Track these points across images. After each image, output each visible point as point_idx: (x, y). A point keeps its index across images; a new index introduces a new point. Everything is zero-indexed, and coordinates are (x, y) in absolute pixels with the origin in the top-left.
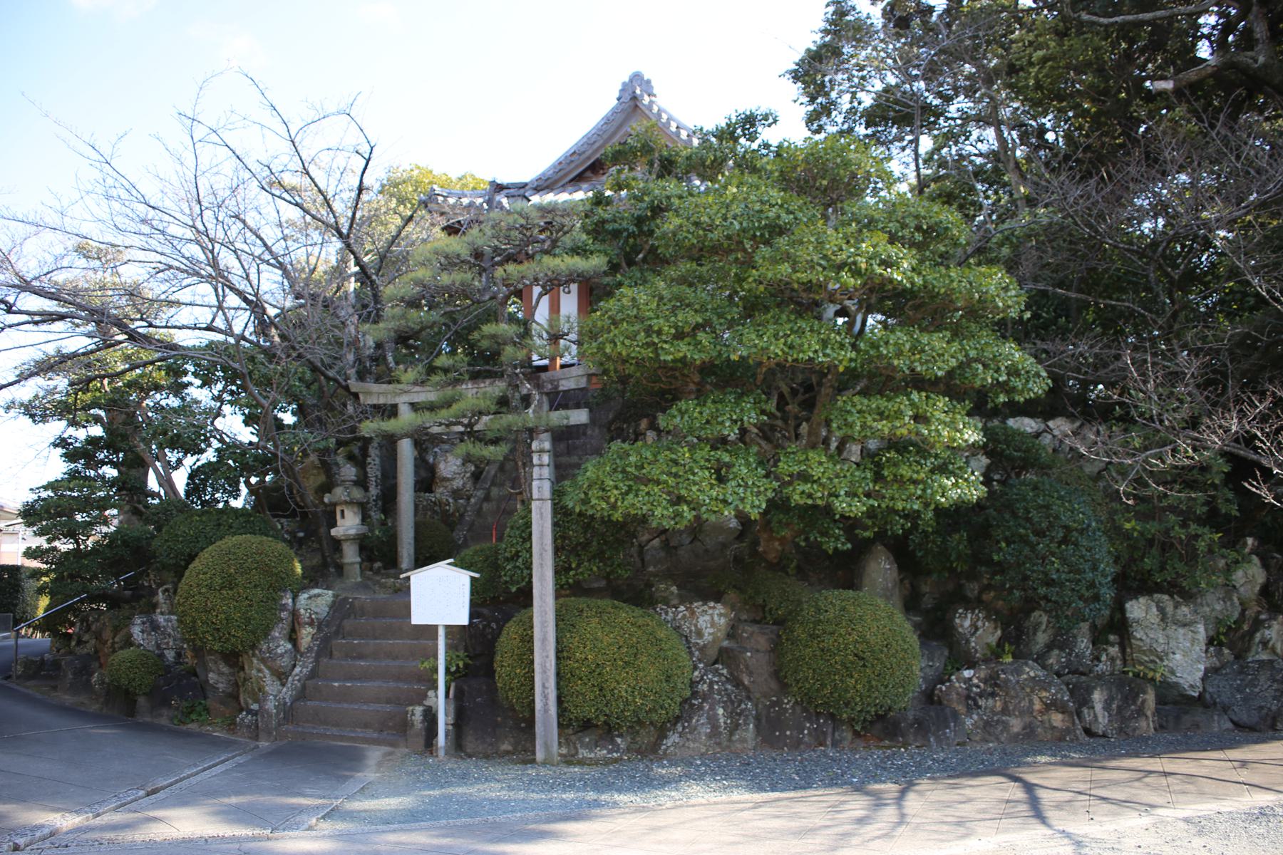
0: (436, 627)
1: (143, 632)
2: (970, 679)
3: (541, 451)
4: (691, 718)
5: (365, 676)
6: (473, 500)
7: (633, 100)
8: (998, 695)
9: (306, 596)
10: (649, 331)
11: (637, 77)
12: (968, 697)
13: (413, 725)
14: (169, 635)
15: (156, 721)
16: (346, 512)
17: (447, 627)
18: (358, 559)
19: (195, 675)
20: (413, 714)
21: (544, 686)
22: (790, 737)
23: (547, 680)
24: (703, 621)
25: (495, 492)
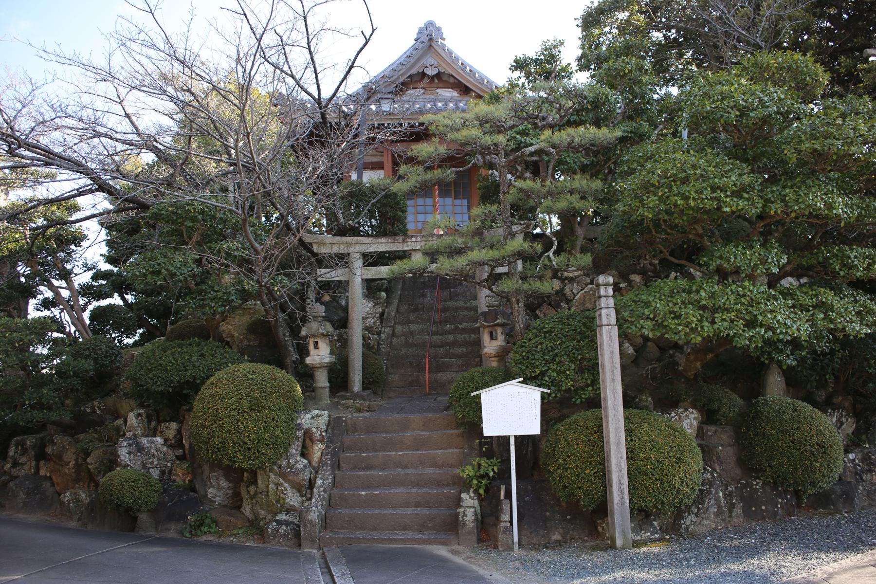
0: (506, 439)
1: (129, 453)
2: (854, 460)
3: (607, 284)
4: (704, 501)
5: (384, 484)
6: (383, 336)
7: (429, 40)
8: (873, 471)
9: (309, 416)
10: (714, 189)
11: (430, 24)
12: (856, 474)
13: (464, 524)
14: (153, 455)
15: (163, 534)
16: (320, 343)
17: (515, 436)
18: (328, 384)
19: (194, 490)
20: (465, 515)
21: (620, 481)
22: (766, 511)
23: (622, 477)
24: (686, 423)
25: (399, 329)
